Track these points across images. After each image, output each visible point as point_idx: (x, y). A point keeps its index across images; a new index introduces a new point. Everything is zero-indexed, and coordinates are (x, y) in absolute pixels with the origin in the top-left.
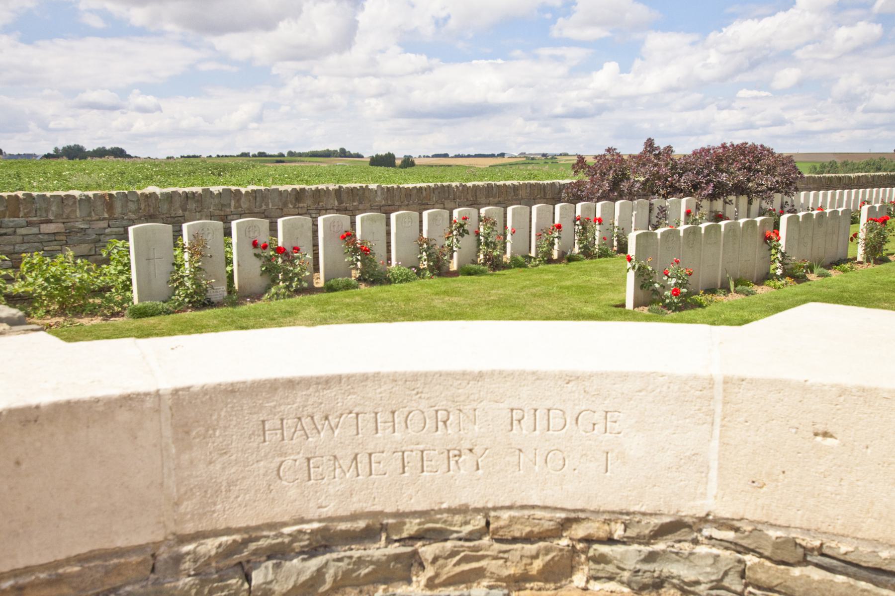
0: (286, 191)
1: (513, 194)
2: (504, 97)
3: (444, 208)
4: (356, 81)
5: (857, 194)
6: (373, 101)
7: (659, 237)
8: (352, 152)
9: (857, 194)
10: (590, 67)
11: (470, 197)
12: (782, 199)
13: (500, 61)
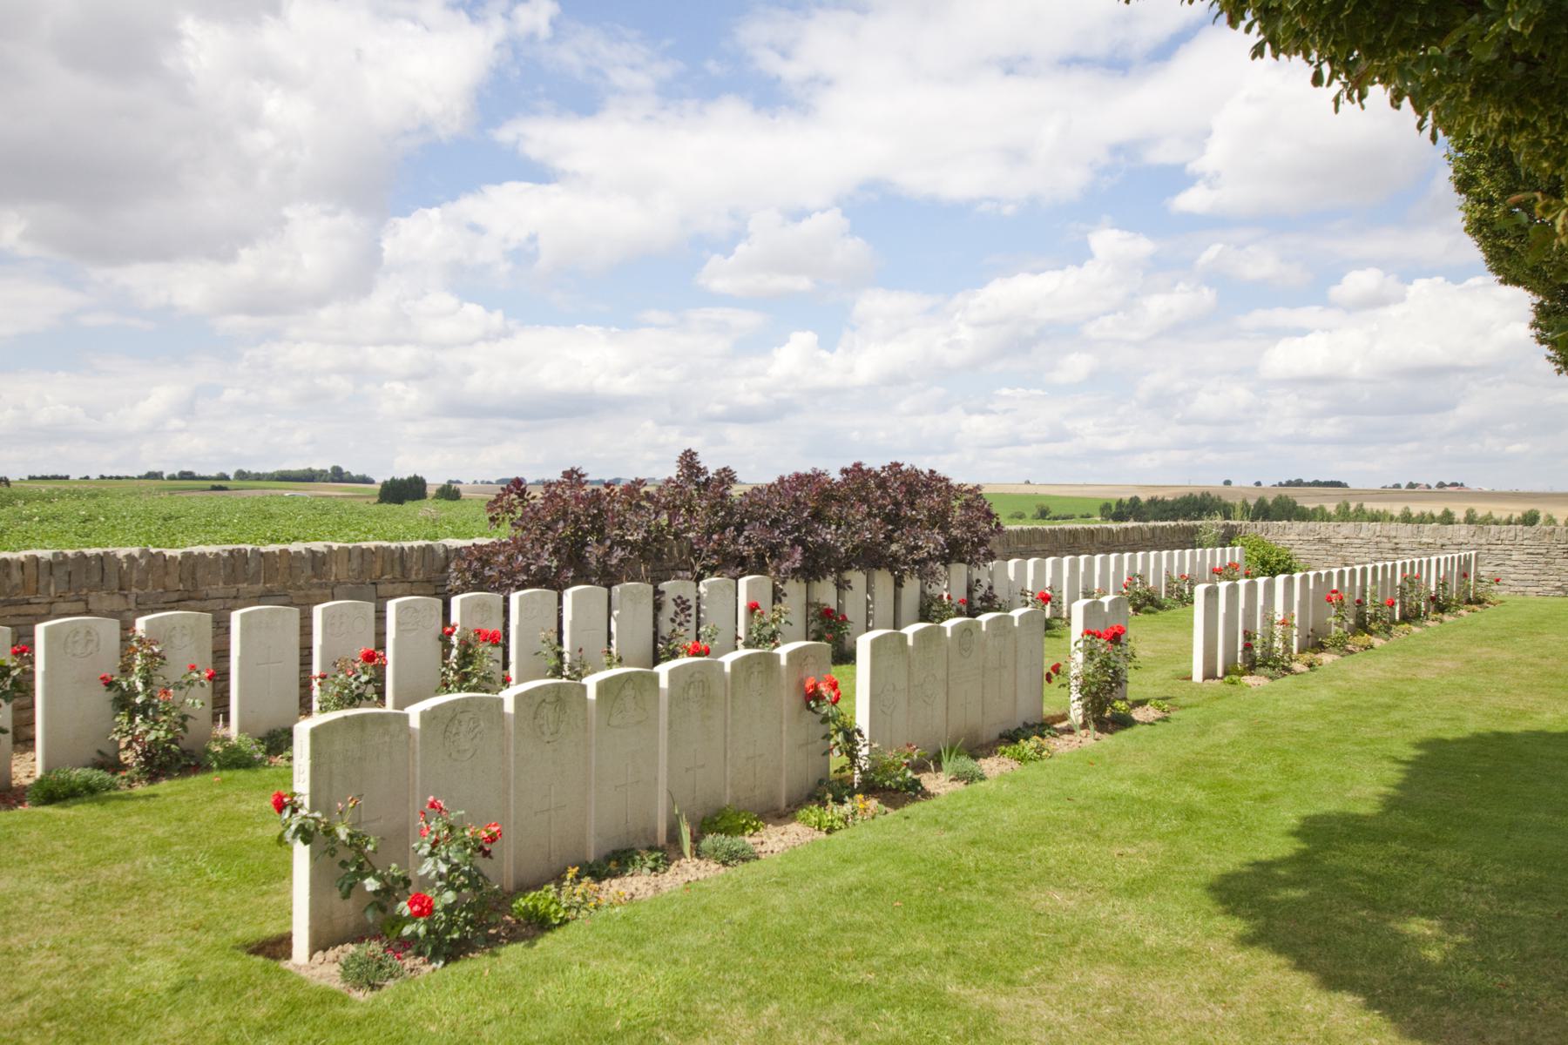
0: (203, 555)
1: (309, 572)
2: (624, 386)
3: (290, 604)
4: (371, 350)
5: (1119, 563)
6: (399, 387)
7: (783, 661)
8: (354, 474)
9: (1119, 563)
10: (762, 344)
11: (172, 581)
12: (969, 576)
13: (613, 329)
